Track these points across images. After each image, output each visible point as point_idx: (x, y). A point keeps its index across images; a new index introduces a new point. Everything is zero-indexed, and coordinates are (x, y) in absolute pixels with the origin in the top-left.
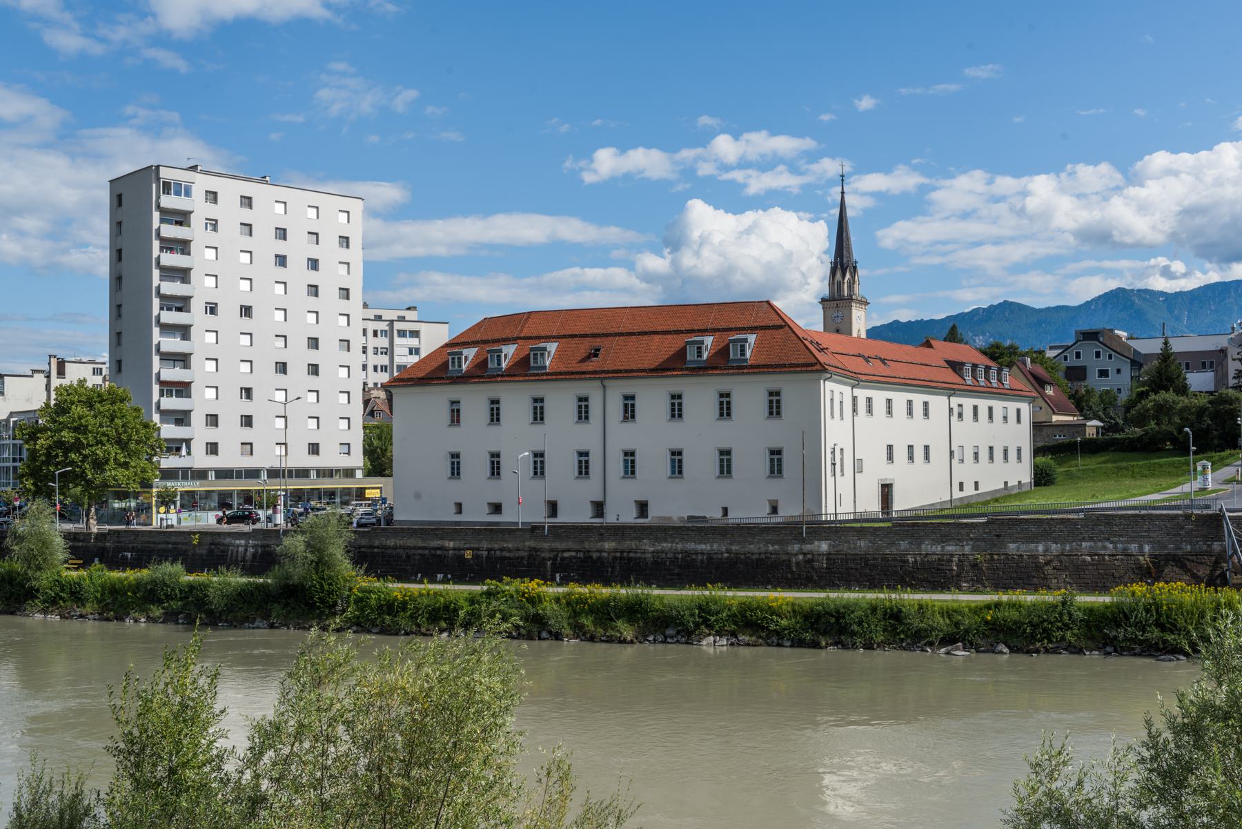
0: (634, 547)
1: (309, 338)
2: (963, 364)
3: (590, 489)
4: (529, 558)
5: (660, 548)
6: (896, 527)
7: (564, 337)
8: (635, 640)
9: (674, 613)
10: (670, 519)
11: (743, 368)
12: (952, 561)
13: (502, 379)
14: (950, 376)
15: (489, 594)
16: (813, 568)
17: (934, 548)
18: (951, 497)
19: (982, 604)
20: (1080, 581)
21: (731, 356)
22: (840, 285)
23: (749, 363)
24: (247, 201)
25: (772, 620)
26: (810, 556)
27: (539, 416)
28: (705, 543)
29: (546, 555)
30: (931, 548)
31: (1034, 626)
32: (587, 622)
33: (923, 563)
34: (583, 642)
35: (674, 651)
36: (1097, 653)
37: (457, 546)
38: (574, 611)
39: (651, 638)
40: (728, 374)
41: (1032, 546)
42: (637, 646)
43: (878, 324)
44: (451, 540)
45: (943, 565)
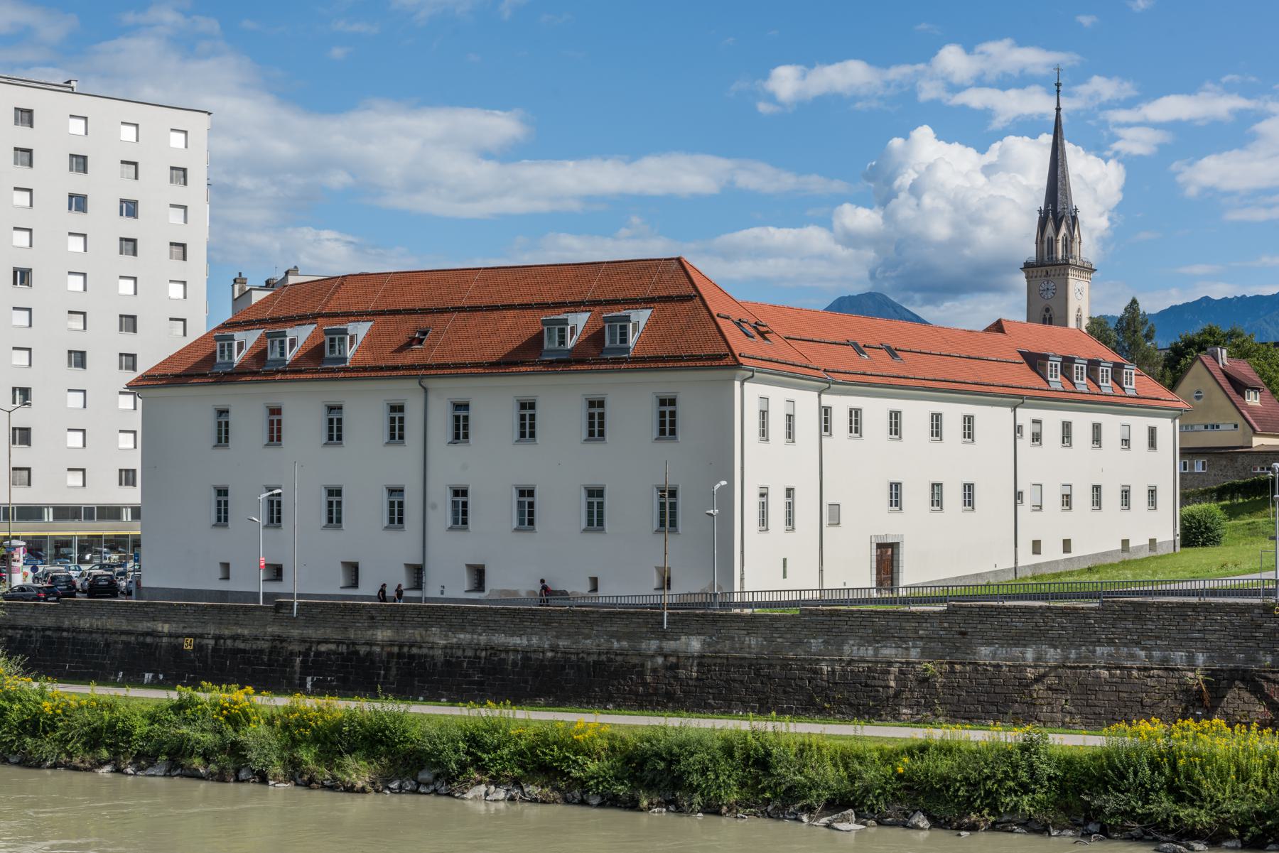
0: (419, 639)
1: (121, 316)
2: (1045, 357)
3: (404, 547)
4: (271, 653)
5: (455, 640)
6: (805, 615)
7: (382, 313)
8: (369, 788)
9: (428, 747)
10: (516, 592)
11: (621, 362)
12: (889, 673)
13: (284, 377)
14: (1025, 376)
15: (179, 707)
16: (676, 678)
17: (862, 651)
18: (1016, 563)
19: (903, 745)
20: (1088, 710)
21: (607, 343)
22: (1052, 244)
23: (631, 354)
24: (25, 116)
25: (575, 762)
26: (673, 660)
27: (596, 428)
28: (520, 636)
29: (296, 647)
30: (857, 651)
31: (973, 785)
32: (307, 755)
33: (844, 675)
34: (299, 788)
35: (428, 805)
36: (1070, 833)
37: (173, 631)
38: (293, 738)
39: (394, 785)
40: (598, 371)
41: (1016, 651)
42: (371, 798)
43: (1180, 303)
44: (166, 622)
45: (874, 678)
